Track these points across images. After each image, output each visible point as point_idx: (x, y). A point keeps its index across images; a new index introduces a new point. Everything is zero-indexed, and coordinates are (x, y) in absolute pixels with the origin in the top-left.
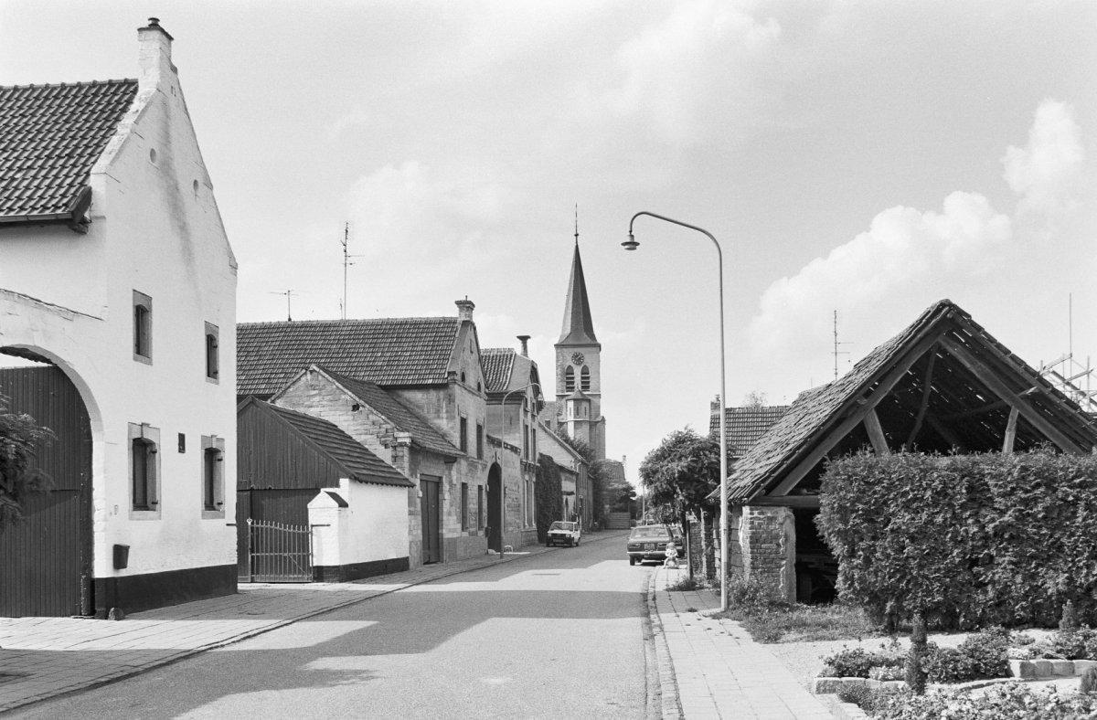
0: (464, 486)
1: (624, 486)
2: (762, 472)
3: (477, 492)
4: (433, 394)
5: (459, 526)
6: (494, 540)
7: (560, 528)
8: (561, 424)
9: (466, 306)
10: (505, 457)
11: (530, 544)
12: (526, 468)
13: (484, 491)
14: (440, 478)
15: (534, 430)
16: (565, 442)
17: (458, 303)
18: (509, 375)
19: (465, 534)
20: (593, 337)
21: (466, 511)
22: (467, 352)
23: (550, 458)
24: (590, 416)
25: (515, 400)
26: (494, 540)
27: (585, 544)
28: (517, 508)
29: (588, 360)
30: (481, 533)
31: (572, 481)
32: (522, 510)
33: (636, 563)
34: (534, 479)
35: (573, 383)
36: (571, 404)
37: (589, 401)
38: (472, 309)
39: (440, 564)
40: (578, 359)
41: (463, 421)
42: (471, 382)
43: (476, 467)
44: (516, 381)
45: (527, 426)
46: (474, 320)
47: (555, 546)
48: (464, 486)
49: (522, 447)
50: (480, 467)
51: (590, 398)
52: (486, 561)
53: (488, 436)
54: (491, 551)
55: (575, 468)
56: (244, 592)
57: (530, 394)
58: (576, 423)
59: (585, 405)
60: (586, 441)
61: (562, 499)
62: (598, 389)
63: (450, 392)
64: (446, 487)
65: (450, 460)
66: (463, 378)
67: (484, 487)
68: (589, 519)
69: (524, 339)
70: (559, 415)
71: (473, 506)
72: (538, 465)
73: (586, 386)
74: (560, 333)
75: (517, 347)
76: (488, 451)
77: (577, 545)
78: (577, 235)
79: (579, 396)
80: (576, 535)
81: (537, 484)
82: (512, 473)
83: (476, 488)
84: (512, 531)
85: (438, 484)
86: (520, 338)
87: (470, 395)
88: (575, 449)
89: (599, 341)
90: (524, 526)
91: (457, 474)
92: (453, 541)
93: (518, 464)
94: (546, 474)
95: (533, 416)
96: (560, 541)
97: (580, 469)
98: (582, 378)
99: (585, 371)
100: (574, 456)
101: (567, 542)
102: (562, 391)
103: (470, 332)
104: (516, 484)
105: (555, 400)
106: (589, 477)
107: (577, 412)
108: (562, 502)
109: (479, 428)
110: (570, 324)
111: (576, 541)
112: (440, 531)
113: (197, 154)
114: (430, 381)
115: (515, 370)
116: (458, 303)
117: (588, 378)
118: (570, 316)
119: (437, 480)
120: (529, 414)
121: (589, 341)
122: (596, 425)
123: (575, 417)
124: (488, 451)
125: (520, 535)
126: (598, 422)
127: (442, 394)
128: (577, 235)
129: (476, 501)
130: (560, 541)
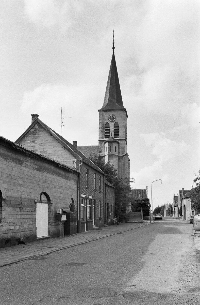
2: (52, 254)
24: (119, 152)
29: (118, 119)
36: (107, 145)
37: (119, 143)
40: (112, 118)
51: (119, 141)
55: (77, 169)
56: (144, 222)
58: (109, 156)
59: (115, 145)
60: (116, 167)
70: (100, 152)
73: (116, 134)
78: (113, 48)
79: (112, 140)
89: (125, 107)
98: (115, 130)
107: (110, 149)
113: (116, 156)
117: (118, 129)
121: (118, 106)
122: (123, 158)
126: (124, 156)
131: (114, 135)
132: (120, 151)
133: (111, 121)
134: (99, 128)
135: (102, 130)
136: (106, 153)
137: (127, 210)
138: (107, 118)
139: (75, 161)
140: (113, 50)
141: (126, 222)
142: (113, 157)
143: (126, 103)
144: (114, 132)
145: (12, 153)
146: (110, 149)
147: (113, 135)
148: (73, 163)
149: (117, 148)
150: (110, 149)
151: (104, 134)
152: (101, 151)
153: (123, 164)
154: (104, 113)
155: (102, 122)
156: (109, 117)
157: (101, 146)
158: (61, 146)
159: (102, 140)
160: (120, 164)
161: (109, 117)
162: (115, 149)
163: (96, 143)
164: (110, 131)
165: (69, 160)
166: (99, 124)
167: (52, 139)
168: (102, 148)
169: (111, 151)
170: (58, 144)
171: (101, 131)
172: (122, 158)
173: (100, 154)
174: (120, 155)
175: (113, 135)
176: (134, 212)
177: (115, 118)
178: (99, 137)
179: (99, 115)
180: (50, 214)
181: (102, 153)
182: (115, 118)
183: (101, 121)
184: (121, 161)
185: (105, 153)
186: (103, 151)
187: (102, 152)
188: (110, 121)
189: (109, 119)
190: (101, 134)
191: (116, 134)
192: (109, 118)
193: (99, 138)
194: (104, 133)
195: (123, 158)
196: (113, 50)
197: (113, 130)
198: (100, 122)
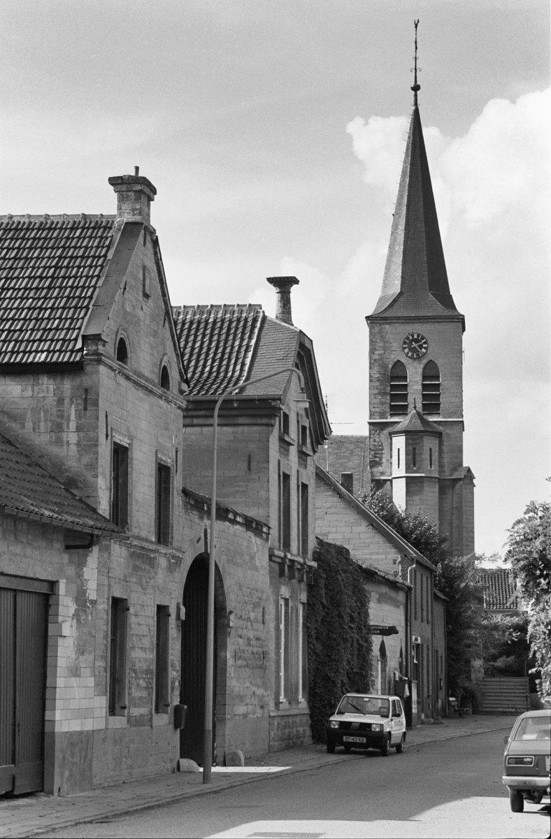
0: (119, 607)
1: (515, 620)
3: (153, 622)
4: (47, 385)
5: (102, 702)
6: (195, 737)
7: (358, 710)
8: (379, 484)
9: (135, 189)
10: (226, 540)
11: (288, 745)
12: (283, 570)
13: (172, 621)
14: (53, 585)
15: (305, 487)
16: (388, 523)
17: (114, 181)
18: (248, 361)
19: (119, 722)
20: (447, 301)
21: (122, 666)
22: (134, 296)
23: (342, 552)
24: (441, 466)
25: (262, 416)
26: (195, 737)
27: (420, 748)
28: (259, 663)
29: (434, 352)
30: (163, 720)
31: (395, 604)
32: (271, 666)
33: (528, 805)
34: (304, 597)
35: (405, 397)
36: (399, 442)
37: (439, 435)
38: (150, 199)
39: (43, 799)
41: (121, 455)
42: (144, 359)
43: (151, 562)
44: (266, 374)
45: (286, 477)
46: (154, 222)
47: (347, 751)
48: (119, 607)
49: (274, 523)
50: (163, 562)
51: (441, 428)
52: (162, 792)
53: (185, 492)
54: (187, 763)
57: (295, 405)
58: (410, 482)
59: (429, 443)
61: (369, 643)
62: (459, 411)
63: (86, 381)
64: (66, 605)
65: (79, 542)
66: (122, 352)
67: (173, 611)
68: (437, 688)
69: (284, 285)
71: (141, 654)
72: (314, 564)
73: (432, 403)
74: (378, 294)
75: (269, 303)
76: (185, 526)
77: (399, 749)
78: (416, 88)
79: (418, 426)
80: (395, 727)
81: (310, 607)
82: (247, 571)
83: (152, 611)
84: (245, 716)
85: (46, 597)
86: (274, 281)
87: (141, 394)
88: (406, 536)
89: (461, 309)
90: (277, 704)
91: (96, 574)
92: (83, 741)
93: (263, 560)
94: (331, 588)
95: (302, 455)
96: (357, 740)
97: (414, 580)
98: (425, 387)
99: (431, 373)
100: (401, 550)
101: (374, 744)
102: (382, 415)
103: (141, 254)
104: (256, 605)
105: (367, 434)
106: (436, 597)
108: (369, 650)
109: (163, 473)
110: (399, 274)
111: (394, 741)
112: (48, 716)
114: (42, 357)
115: (260, 351)
116: (114, 181)
118: (399, 259)
119: (44, 589)
120: (293, 450)
121: (440, 310)
123: (407, 471)
124: (185, 526)
125: (265, 724)
126: (460, 479)
127: (67, 385)
128: (416, 88)
129: (149, 641)
130: (357, 740)
131: (423, 404)
132: (446, 460)
133: (413, 355)
134: (371, 381)
135: (382, 387)
136: (401, 471)
137: (473, 670)
138: (396, 345)
139: (399, 560)
140: (416, 95)
141: (476, 712)
142: (423, 486)
143: (464, 290)
144: (424, 395)
145: (155, 505)
146: (414, 458)
147: (419, 406)
148: (395, 564)
149: (437, 454)
150: (410, 457)
151: (388, 401)
152: (377, 459)
153: (457, 508)
154: (387, 326)
155: (381, 359)
156: (405, 343)
157: (376, 444)
158: (364, 523)
159: (382, 420)
160: (447, 507)
161: (405, 343)
162: (429, 457)
163: (364, 431)
164: (410, 390)
165: (384, 556)
166: (370, 363)
167: (342, 505)
168: (382, 450)
169: (414, 465)
170: (357, 517)
171: (376, 391)
172: (453, 487)
173: (375, 470)
174: (447, 476)
175: (421, 405)
176: (186, 720)
177: (425, 348)
178: (370, 411)
179: (371, 333)
180: (385, 682)
181: (380, 469)
182: (425, 348)
183: (376, 357)
184: (450, 496)
185: (397, 469)
186: (384, 460)
187: (380, 464)
188: (407, 356)
189: (406, 350)
190: (376, 401)
191: (432, 403)
192: (406, 346)
193: (371, 415)
194: (388, 397)
195: (457, 486)
196: (416, 95)
197: (420, 387)
198: (375, 360)
